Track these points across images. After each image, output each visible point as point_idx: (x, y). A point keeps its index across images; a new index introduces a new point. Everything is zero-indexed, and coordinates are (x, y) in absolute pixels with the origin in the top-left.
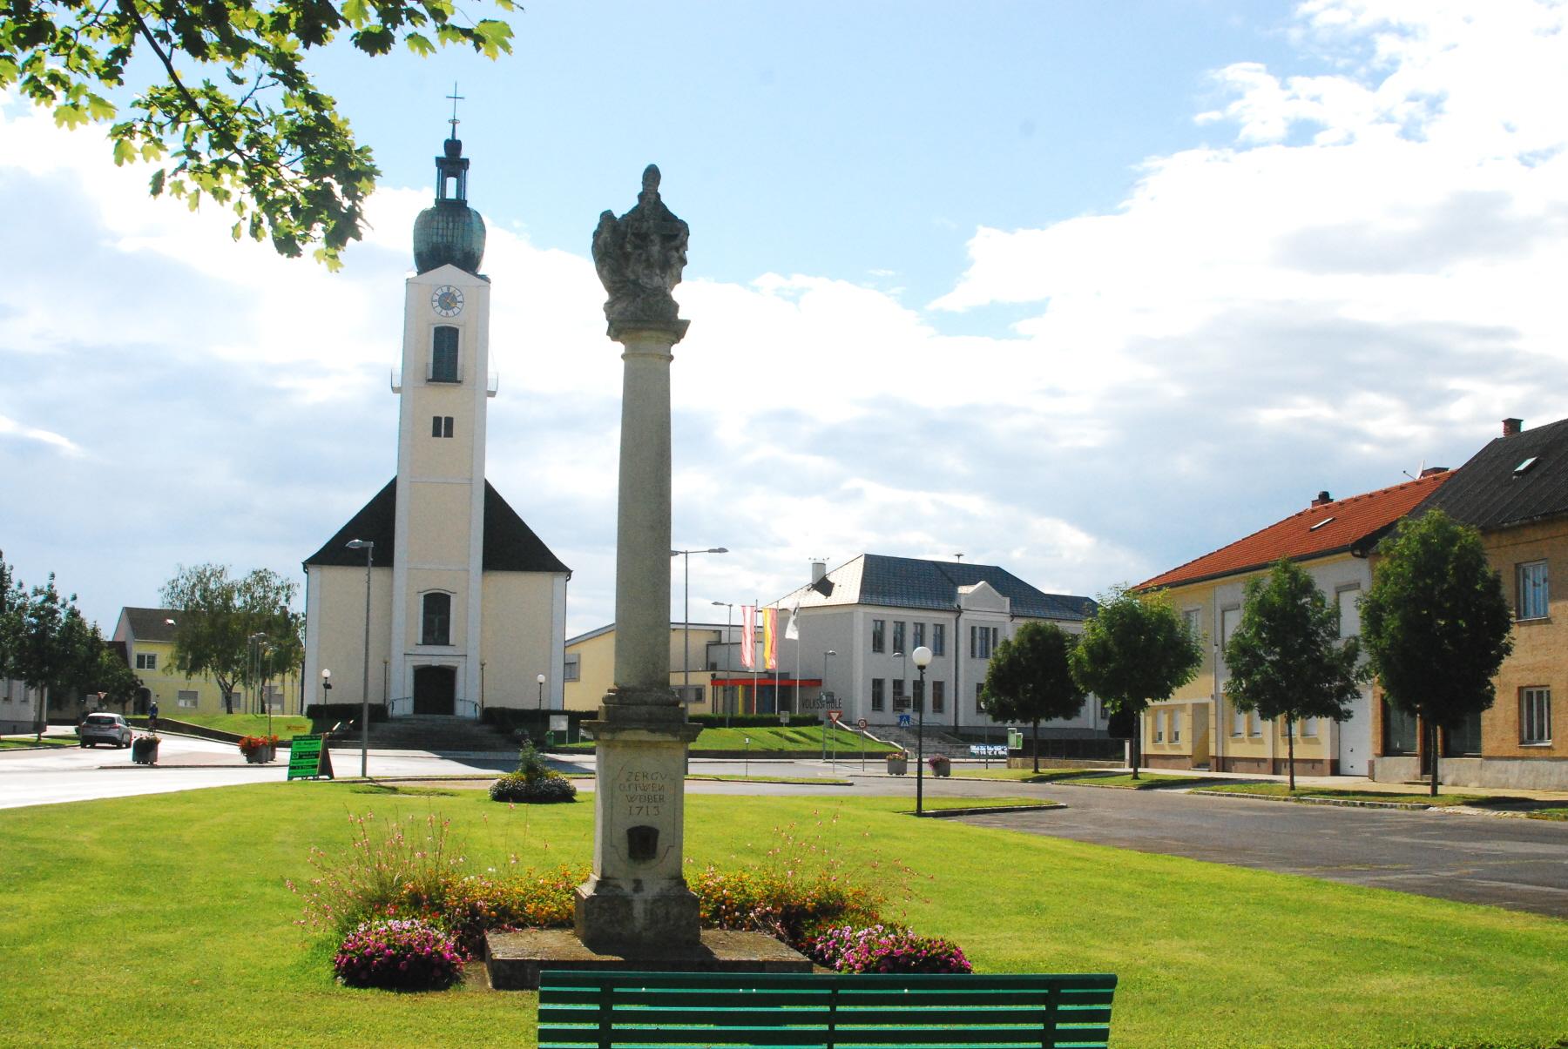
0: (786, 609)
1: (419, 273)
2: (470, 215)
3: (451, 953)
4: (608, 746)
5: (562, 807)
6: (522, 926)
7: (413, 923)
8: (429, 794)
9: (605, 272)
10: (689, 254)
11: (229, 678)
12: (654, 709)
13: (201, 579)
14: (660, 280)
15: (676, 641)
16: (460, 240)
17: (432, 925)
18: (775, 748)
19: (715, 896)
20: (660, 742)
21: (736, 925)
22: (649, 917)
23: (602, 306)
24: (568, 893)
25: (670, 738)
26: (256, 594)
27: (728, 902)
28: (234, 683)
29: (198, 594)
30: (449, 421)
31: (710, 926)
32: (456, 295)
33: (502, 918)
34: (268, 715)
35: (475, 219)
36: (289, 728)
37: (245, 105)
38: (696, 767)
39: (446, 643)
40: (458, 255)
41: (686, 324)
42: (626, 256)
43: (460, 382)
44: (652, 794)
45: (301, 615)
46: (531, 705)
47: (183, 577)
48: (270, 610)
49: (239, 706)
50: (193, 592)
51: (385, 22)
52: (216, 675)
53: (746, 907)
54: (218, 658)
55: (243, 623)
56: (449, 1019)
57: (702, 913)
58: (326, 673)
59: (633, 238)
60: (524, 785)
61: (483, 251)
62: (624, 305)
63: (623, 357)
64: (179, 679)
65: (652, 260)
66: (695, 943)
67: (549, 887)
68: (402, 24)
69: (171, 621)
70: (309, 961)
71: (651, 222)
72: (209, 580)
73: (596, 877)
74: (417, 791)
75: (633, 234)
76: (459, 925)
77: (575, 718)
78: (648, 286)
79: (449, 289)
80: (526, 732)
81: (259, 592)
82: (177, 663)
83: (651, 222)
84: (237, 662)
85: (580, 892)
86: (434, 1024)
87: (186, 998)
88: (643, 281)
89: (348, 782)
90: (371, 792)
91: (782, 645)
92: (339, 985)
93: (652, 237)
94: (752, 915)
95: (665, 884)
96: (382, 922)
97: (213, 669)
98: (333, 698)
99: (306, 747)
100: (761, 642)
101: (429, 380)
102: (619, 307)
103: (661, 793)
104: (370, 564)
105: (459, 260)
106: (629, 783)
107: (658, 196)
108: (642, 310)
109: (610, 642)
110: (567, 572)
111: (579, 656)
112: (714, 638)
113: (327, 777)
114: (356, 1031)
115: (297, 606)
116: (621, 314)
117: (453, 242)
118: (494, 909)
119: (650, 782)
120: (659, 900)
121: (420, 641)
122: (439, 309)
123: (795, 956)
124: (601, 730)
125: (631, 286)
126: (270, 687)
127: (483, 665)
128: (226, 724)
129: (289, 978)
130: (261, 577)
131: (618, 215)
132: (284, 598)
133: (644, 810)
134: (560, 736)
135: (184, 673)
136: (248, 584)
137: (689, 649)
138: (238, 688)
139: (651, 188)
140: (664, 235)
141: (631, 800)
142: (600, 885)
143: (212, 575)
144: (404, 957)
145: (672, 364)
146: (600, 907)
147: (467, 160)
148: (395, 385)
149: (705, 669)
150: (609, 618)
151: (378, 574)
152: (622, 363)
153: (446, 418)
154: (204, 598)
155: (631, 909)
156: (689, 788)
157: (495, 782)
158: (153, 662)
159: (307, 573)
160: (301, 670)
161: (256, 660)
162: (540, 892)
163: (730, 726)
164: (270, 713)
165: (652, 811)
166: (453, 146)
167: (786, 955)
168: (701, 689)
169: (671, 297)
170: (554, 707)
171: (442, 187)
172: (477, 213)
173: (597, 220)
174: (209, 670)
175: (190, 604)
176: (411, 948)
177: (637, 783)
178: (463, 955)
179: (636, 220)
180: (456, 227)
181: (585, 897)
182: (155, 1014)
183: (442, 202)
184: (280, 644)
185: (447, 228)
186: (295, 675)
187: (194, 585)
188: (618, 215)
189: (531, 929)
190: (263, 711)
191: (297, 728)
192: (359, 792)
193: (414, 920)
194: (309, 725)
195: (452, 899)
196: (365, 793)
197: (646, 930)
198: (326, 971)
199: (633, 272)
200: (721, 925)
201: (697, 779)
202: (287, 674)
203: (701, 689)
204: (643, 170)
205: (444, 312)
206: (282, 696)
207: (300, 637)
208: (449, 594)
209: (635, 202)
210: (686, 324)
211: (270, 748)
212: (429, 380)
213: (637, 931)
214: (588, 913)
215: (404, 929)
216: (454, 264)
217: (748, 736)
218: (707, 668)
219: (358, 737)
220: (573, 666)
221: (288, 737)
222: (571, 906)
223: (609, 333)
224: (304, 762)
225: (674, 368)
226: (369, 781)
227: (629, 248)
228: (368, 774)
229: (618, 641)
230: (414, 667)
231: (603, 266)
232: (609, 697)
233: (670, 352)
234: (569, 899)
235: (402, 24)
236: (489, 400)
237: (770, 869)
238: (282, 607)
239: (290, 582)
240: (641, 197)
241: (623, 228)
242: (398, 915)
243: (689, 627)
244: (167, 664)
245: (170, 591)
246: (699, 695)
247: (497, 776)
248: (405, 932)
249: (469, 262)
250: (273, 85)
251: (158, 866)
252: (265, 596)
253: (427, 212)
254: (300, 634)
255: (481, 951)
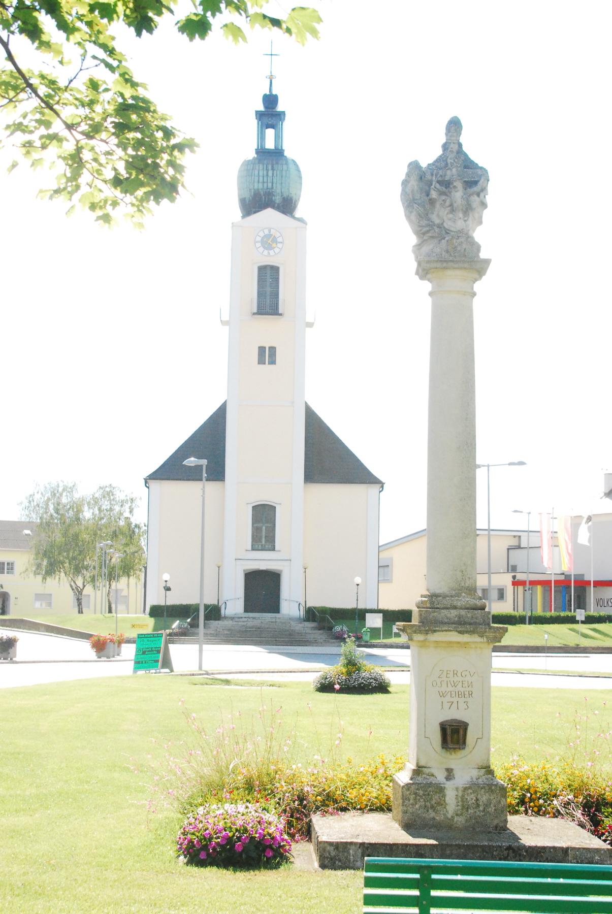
0: (581, 516)
1: (243, 217)
2: (287, 164)
3: (281, 834)
4: (421, 647)
5: (378, 697)
6: (344, 810)
7: (247, 807)
8: (261, 684)
9: (413, 217)
10: (489, 199)
11: (79, 582)
12: (463, 612)
13: (55, 494)
14: (463, 222)
15: (481, 544)
16: (279, 186)
17: (264, 809)
18: (572, 644)
19: (521, 785)
20: (468, 642)
21: (539, 812)
22: (460, 804)
23: (411, 249)
24: (386, 779)
25: (476, 638)
26: (104, 507)
27: (532, 791)
28: (84, 586)
29: (51, 507)
30: (273, 350)
31: (517, 812)
32: (277, 236)
33: (327, 802)
34: (115, 615)
35: (291, 166)
36: (133, 626)
37: (72, 85)
38: (500, 661)
39: (273, 549)
40: (278, 199)
41: (487, 262)
42: (432, 202)
43: (281, 315)
44: (462, 690)
45: (143, 525)
46: (347, 603)
47: (38, 493)
48: (117, 522)
49: (89, 607)
50: (47, 505)
51: (205, 10)
52: (68, 579)
53: (549, 796)
54: (70, 564)
55: (92, 533)
56: (280, 897)
57: (509, 800)
58: (166, 577)
59: (438, 186)
60: (344, 678)
61: (300, 196)
62: (431, 247)
63: (430, 294)
64: (35, 583)
65: (455, 205)
66: (502, 829)
67: (369, 774)
68: (221, 12)
69: (27, 532)
70: (154, 841)
71: (454, 170)
72: (61, 495)
73: (412, 766)
74: (248, 683)
75: (438, 182)
76: (288, 809)
77: (391, 617)
78: (453, 229)
79: (269, 253)
80: (345, 629)
81: (106, 505)
82: (34, 569)
83: (454, 170)
84: (87, 568)
85: (397, 779)
86: (267, 902)
87: (44, 877)
88: (448, 224)
89: (186, 675)
90: (207, 684)
91: (577, 549)
92: (181, 864)
93: (455, 184)
94: (555, 802)
95: (475, 773)
96: (219, 805)
97: (65, 573)
98: (174, 599)
99: (148, 644)
100: (558, 546)
101: (254, 314)
102: (426, 249)
103: (470, 689)
104: (204, 479)
105: (278, 204)
106: (441, 680)
107: (460, 145)
108: (447, 252)
109: (422, 545)
110: (381, 484)
111: (392, 559)
112: (514, 542)
113: (167, 670)
114: (196, 907)
115: (139, 517)
116: (428, 255)
117: (272, 188)
118: (319, 794)
119: (460, 679)
120: (470, 788)
121: (250, 548)
122: (261, 249)
123: (596, 843)
124: (415, 632)
125: (437, 230)
126: (117, 590)
127: (305, 569)
128: (77, 623)
129: (136, 858)
130: (108, 493)
131: (424, 164)
132: (128, 510)
133: (455, 705)
134: (375, 632)
135: (40, 578)
136: (96, 498)
137: (492, 556)
138: (88, 590)
139: (454, 138)
140: (465, 181)
141: (442, 695)
142: (418, 772)
143: (64, 490)
144: (239, 838)
145: (475, 299)
146: (415, 794)
147: (284, 113)
148: (223, 319)
149: (506, 571)
150: (422, 524)
151: (212, 487)
152: (429, 300)
153: (269, 348)
154: (57, 511)
155: (444, 796)
156: (496, 680)
157: (318, 674)
158: (12, 569)
159: (148, 488)
160: (143, 574)
161: (103, 566)
162: (360, 779)
163: (530, 623)
164: (116, 613)
165: (462, 706)
166: (270, 100)
167: (588, 842)
168: (503, 589)
169: (473, 238)
170: (369, 607)
171: (261, 137)
172: (293, 160)
173: (405, 170)
174: (63, 574)
175: (45, 516)
176: (246, 830)
177: (448, 680)
178: (292, 836)
179: (441, 169)
180: (275, 175)
181: (402, 784)
182: (16, 893)
183: (262, 152)
184: (125, 551)
185: (267, 175)
186: (138, 578)
187: (49, 499)
188: (424, 164)
189: (352, 813)
190: (110, 611)
191: (141, 626)
192: (196, 684)
193: (248, 804)
194: (151, 622)
195: (282, 786)
196: (202, 684)
197: (457, 815)
198: (170, 850)
199: (438, 215)
200: (526, 812)
201: (501, 672)
202: (131, 578)
203: (503, 589)
204: (446, 123)
205: (266, 252)
206: (127, 597)
207: (143, 544)
208: (274, 505)
209: (439, 152)
210: (487, 262)
211: (116, 644)
212: (254, 314)
213: (449, 816)
214: (405, 798)
215: (239, 813)
216: (273, 207)
217: (549, 633)
218: (508, 571)
219: (193, 634)
220: (386, 569)
221: (133, 634)
222: (389, 791)
223: (417, 273)
224: (147, 657)
225: (477, 304)
226: (205, 674)
227: (434, 194)
228: (204, 668)
229: (431, 549)
230: (244, 570)
231: (411, 212)
232: (422, 602)
233: (473, 289)
234: (387, 785)
235: (221, 12)
236: (308, 329)
237: (570, 761)
238: (127, 518)
239: (133, 496)
240: (445, 147)
241: (428, 177)
242: (233, 799)
243: (492, 533)
244: (24, 569)
245: (27, 504)
246: (501, 595)
247: (318, 670)
248: (239, 815)
249: (287, 206)
250: (96, 66)
251: (19, 754)
252: (111, 508)
253: (249, 161)
254: (143, 543)
255: (308, 832)
